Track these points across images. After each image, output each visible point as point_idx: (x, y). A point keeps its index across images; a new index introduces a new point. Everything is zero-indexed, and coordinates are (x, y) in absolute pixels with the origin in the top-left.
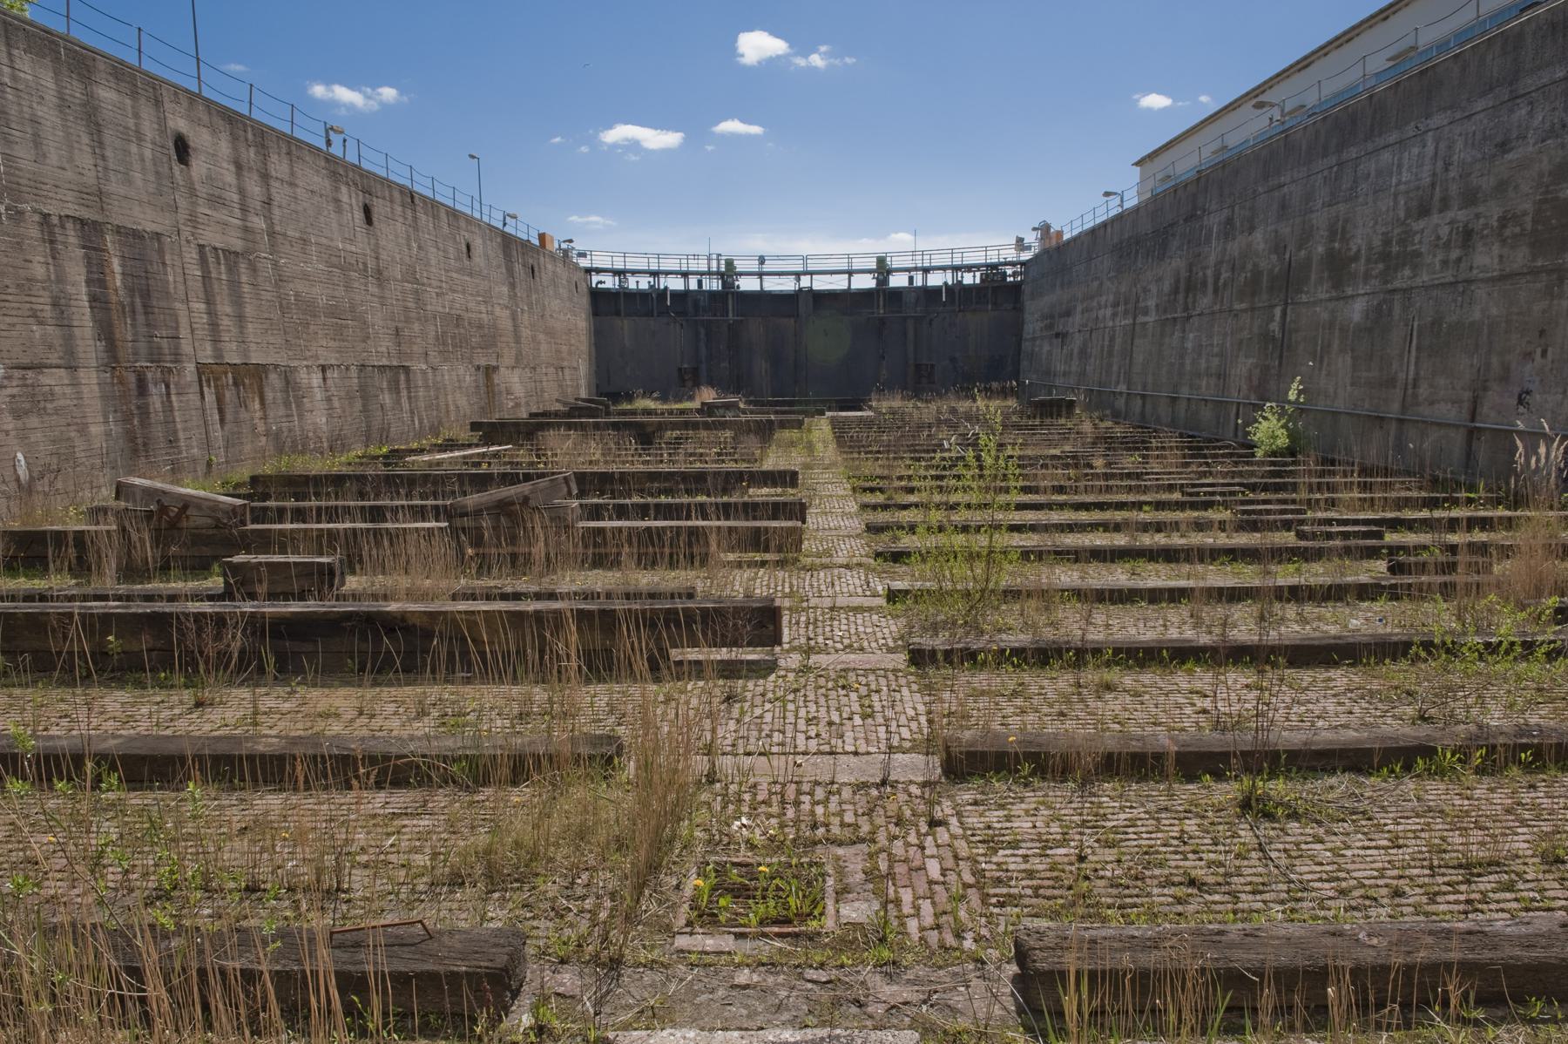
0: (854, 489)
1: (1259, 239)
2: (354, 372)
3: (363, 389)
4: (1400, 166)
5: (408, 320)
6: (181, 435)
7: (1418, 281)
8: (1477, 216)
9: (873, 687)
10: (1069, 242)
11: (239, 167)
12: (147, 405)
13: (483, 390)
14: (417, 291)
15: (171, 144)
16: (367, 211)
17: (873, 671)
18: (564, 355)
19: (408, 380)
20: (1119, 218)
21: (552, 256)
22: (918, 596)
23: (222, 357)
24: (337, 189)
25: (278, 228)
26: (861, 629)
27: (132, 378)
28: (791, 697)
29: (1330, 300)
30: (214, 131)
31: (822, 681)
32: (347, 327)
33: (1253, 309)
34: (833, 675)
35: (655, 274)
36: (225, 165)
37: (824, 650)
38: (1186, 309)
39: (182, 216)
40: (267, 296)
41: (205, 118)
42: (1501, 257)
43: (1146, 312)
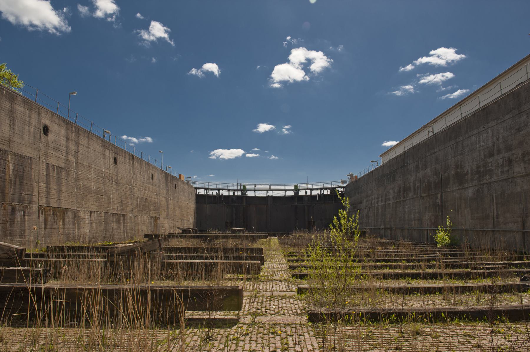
0: (285, 256)
1: (429, 171)
2: (103, 214)
3: (106, 221)
4: (479, 141)
5: (126, 198)
6: (27, 231)
7: (493, 180)
8: (513, 154)
9: (289, 333)
10: (360, 179)
11: (67, 139)
12: (14, 219)
13: (153, 225)
14: (131, 188)
15: (42, 128)
16: (115, 160)
17: (289, 325)
18: (185, 216)
19: (124, 219)
20: (377, 169)
21: (183, 181)
22: (311, 291)
23: (50, 204)
24: (105, 151)
25: (80, 161)
26: (284, 305)
27: (10, 208)
28: (242, 338)
29: (459, 189)
30: (60, 126)
31: (261, 330)
32: (102, 198)
33: (429, 195)
34: (268, 327)
35: (219, 190)
36: (62, 138)
37: (265, 314)
38: (404, 197)
39: (41, 153)
40: (72, 184)
41: (57, 121)
42: (525, 168)
43: (389, 200)
